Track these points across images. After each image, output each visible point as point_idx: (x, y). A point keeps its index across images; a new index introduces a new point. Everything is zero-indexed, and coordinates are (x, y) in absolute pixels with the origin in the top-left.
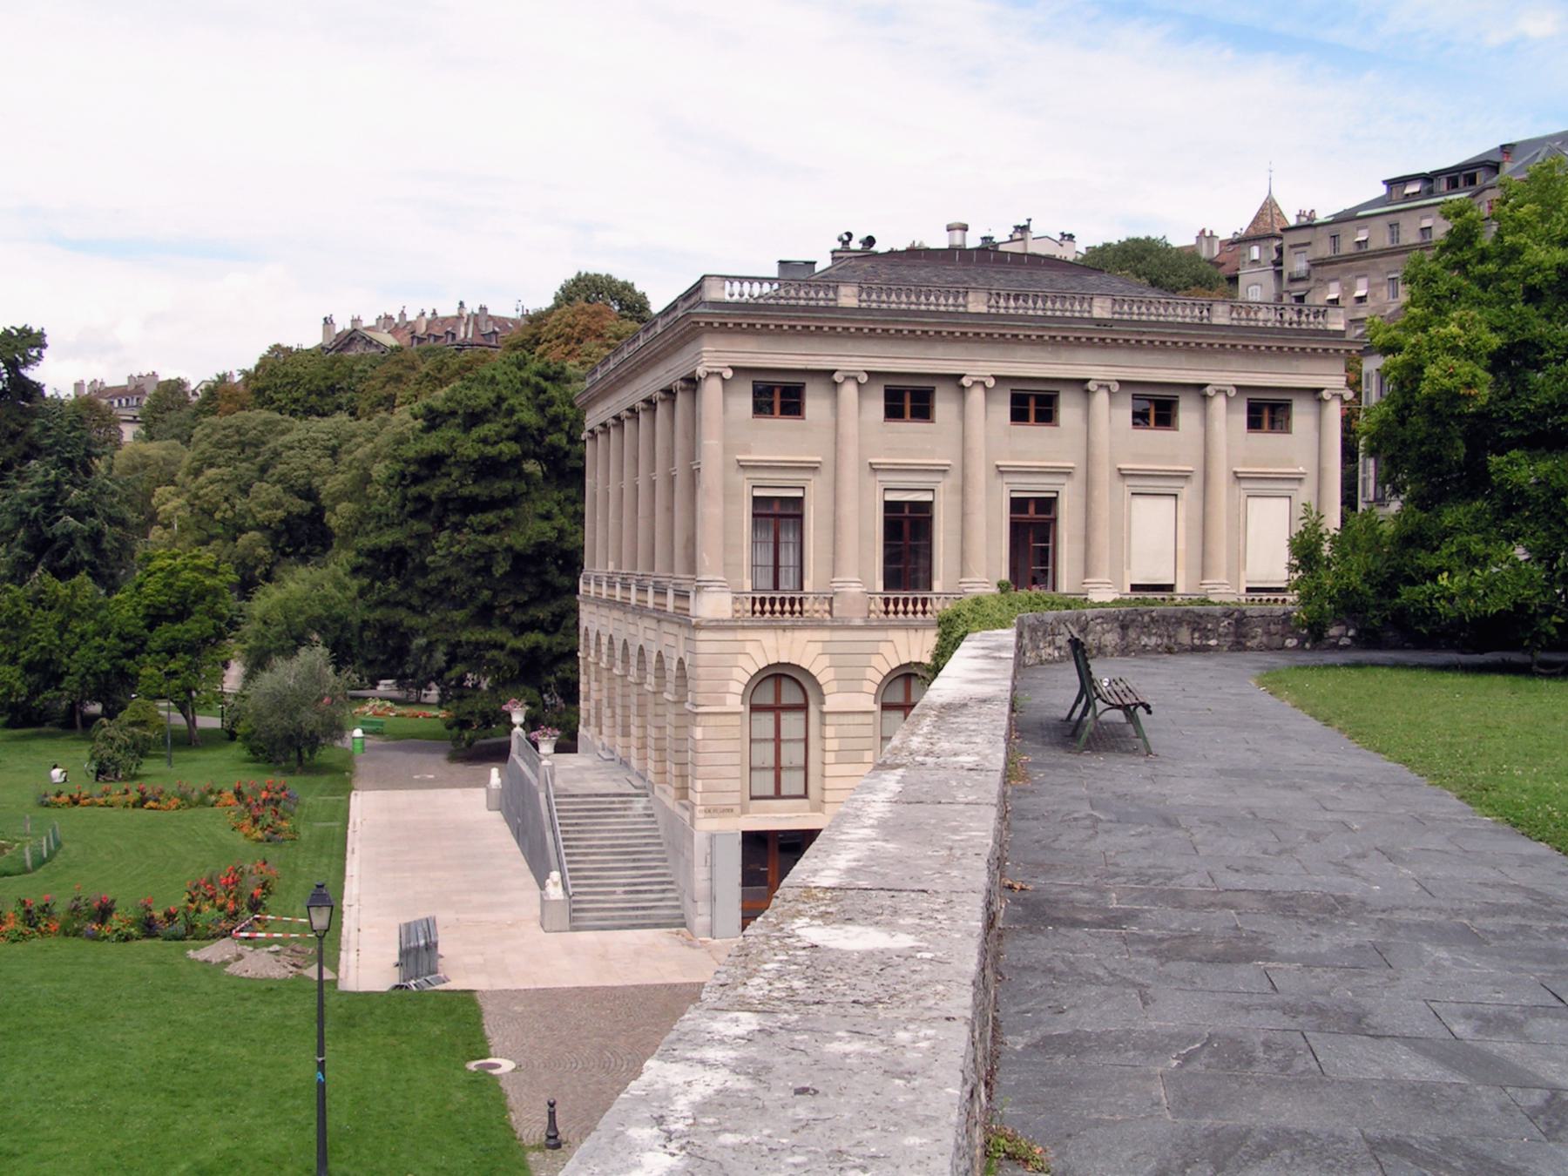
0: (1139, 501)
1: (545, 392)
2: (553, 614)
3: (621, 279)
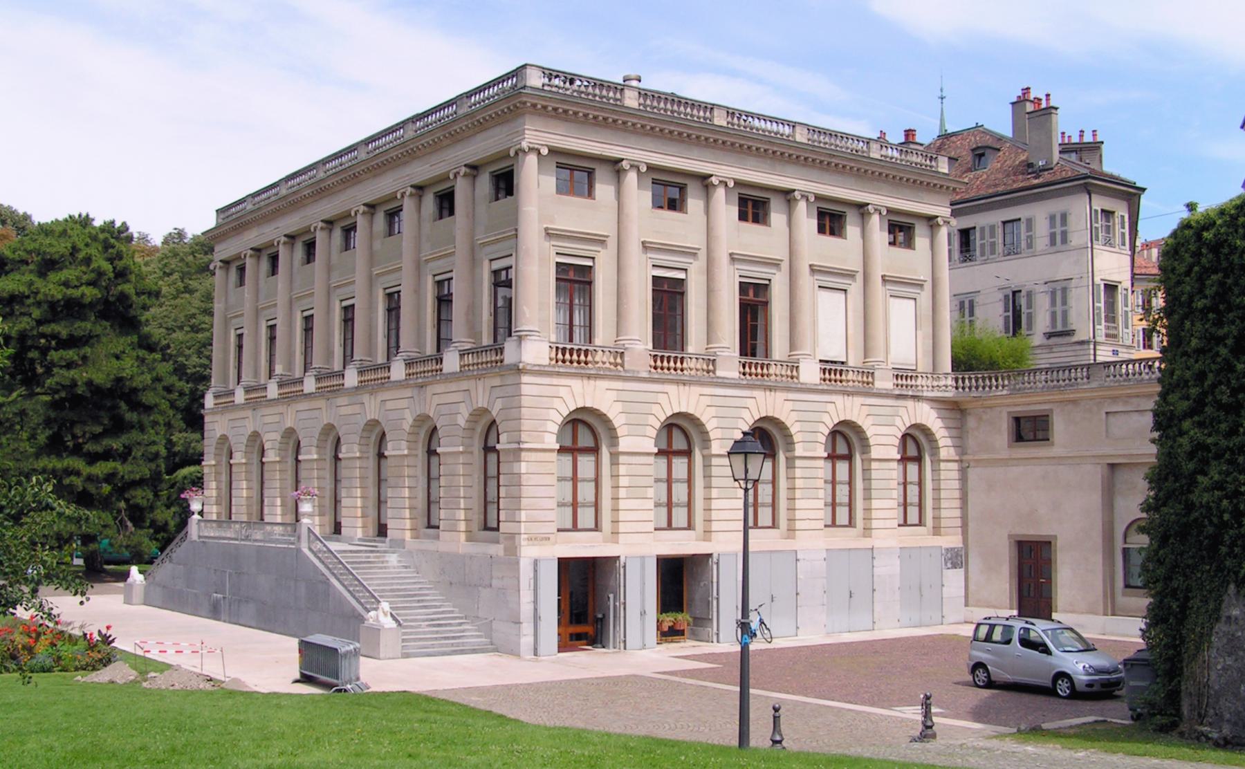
0: (824, 294)
1: (113, 247)
2: (124, 446)
3: (21, 212)
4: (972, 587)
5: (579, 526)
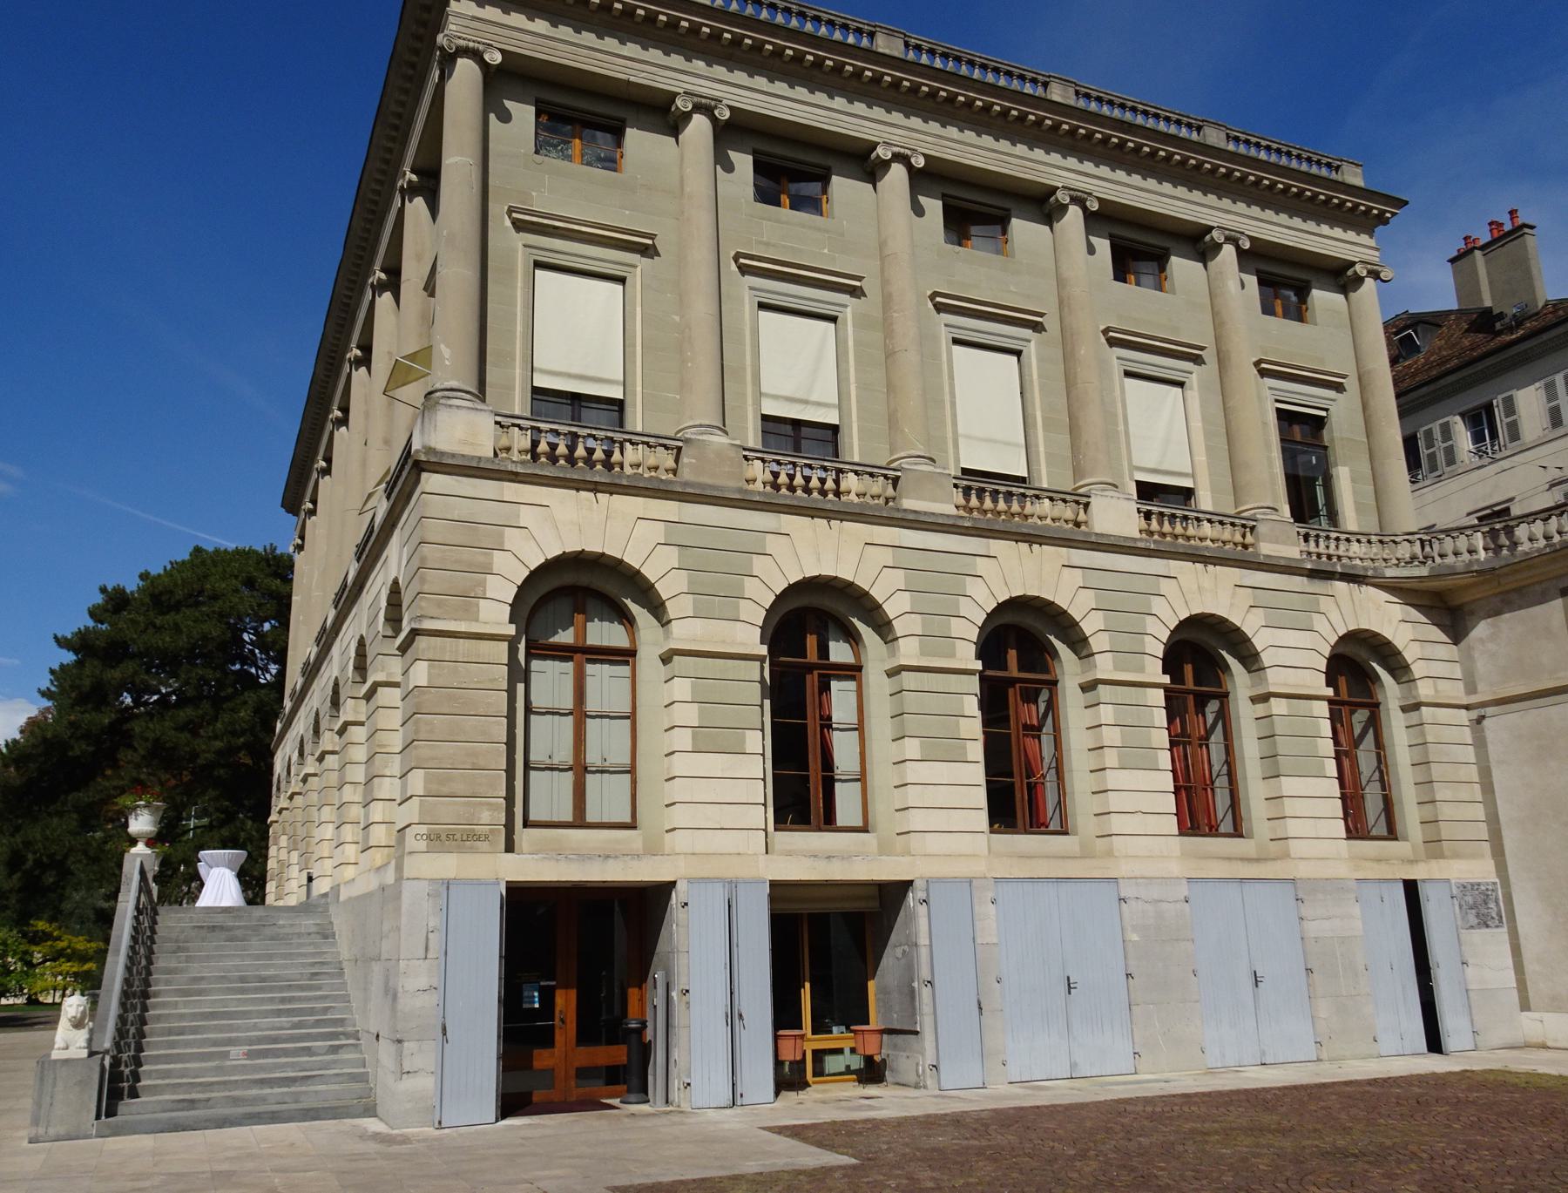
4: (1530, 967)
5: (590, 818)
